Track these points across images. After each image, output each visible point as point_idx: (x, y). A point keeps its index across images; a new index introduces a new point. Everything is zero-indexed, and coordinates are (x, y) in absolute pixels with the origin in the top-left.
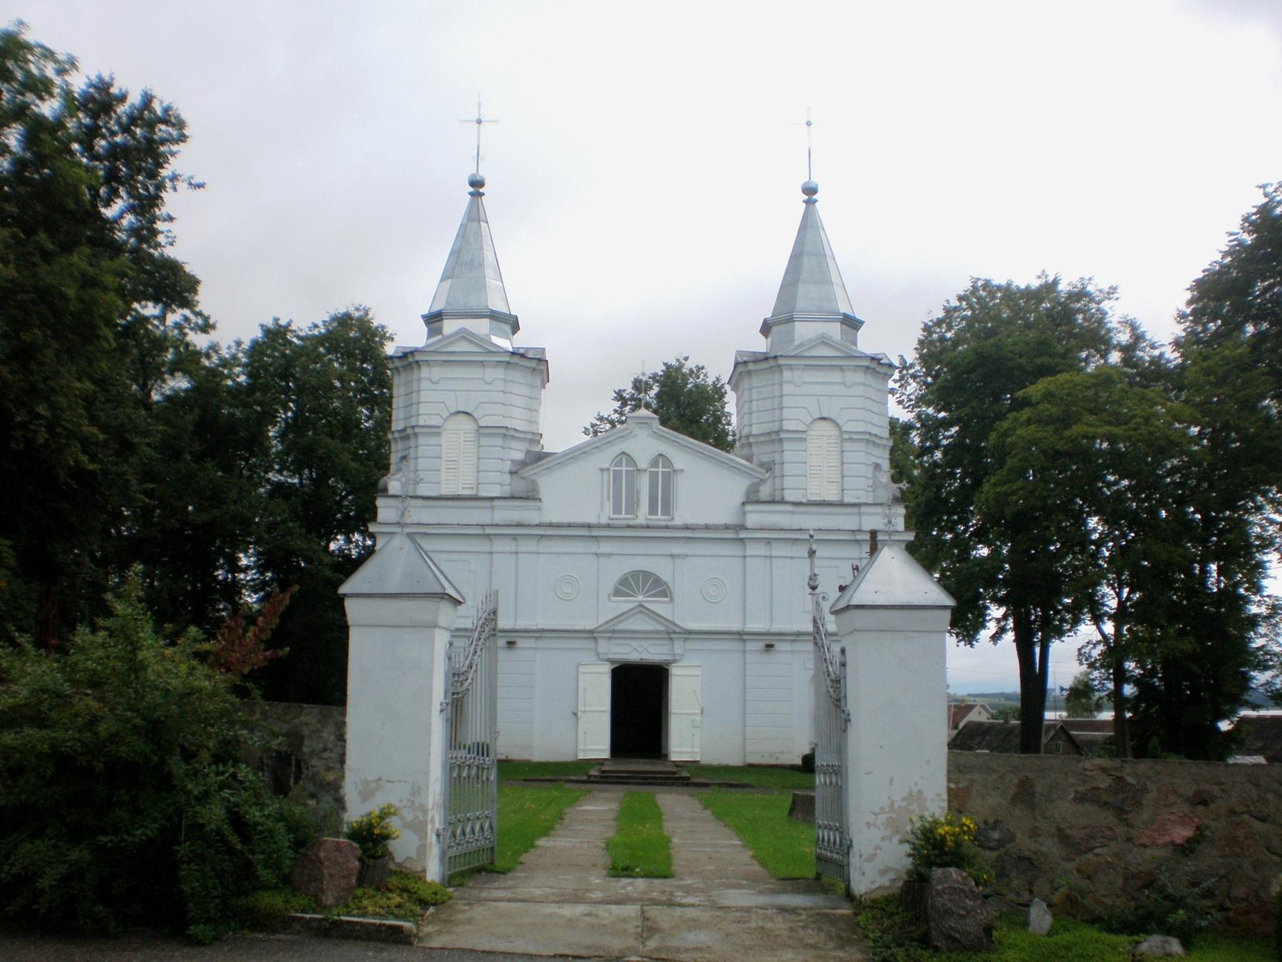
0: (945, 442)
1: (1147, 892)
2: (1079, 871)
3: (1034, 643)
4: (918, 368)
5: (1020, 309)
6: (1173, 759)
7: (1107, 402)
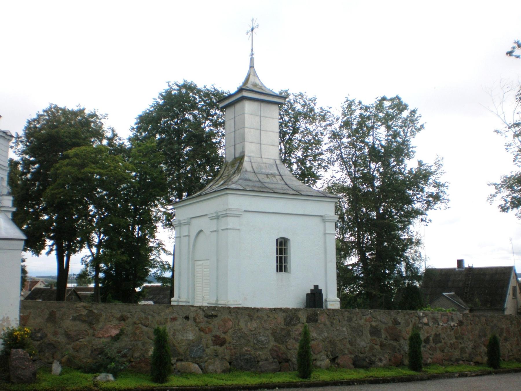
0: (32, 170)
1: (100, 356)
2: (74, 349)
3: (63, 256)
4: (23, 138)
5: (68, 118)
6: (117, 302)
7: (100, 159)
